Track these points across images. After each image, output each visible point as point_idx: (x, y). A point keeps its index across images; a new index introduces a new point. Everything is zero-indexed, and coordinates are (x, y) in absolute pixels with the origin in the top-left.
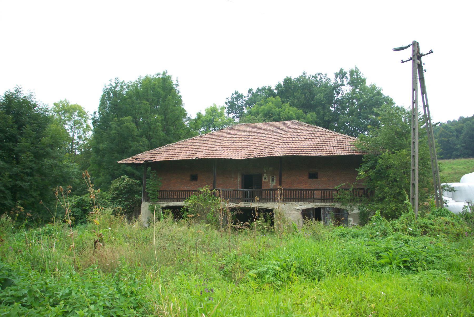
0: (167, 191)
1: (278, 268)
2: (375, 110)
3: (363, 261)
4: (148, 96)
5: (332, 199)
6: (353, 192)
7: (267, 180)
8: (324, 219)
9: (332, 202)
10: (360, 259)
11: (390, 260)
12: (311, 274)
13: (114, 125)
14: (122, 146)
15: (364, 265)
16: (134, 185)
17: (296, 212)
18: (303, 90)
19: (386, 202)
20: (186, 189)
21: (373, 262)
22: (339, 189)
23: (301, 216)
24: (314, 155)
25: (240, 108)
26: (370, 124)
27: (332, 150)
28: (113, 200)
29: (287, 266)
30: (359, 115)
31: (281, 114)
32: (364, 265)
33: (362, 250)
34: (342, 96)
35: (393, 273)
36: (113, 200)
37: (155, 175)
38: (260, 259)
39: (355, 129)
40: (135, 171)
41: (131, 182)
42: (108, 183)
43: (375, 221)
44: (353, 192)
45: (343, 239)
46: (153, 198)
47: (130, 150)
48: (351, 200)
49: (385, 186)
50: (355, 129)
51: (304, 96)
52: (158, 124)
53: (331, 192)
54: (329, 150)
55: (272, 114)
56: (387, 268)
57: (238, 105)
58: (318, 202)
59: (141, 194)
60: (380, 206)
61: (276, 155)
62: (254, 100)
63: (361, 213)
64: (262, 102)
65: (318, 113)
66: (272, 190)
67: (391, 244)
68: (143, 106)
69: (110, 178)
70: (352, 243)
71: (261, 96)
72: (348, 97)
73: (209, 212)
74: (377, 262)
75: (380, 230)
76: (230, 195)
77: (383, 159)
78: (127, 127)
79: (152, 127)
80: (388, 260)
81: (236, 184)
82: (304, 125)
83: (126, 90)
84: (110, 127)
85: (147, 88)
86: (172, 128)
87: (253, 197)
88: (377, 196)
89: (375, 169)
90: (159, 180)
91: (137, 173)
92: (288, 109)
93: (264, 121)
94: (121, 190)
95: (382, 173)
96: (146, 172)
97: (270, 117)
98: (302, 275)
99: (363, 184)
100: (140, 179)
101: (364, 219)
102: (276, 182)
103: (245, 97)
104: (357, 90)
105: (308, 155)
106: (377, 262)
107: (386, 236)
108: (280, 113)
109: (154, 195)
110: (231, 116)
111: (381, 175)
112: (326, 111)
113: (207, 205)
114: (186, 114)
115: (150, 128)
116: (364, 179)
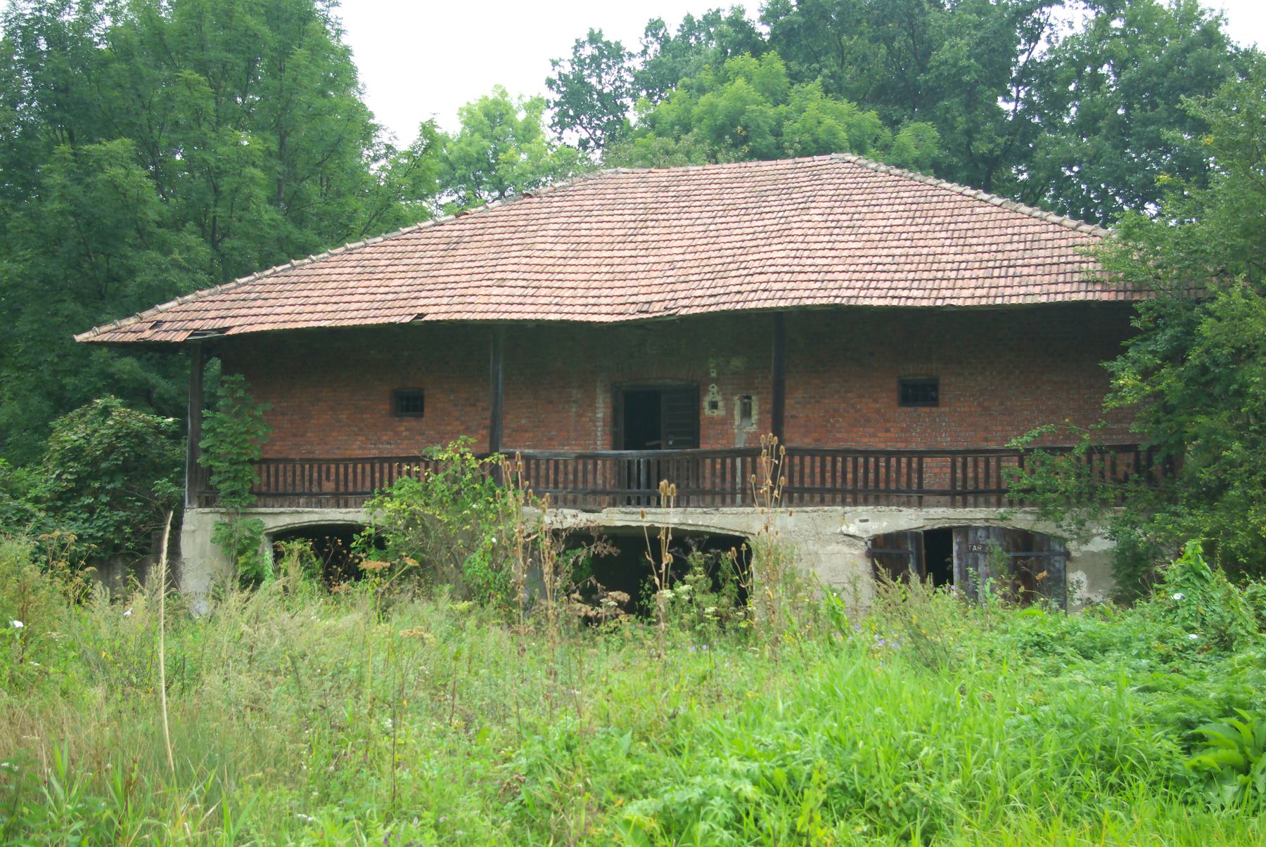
0: (292, 461)
1: (748, 790)
2: (1191, 104)
3: (1124, 760)
4: (202, 48)
5: (1000, 492)
6: (1090, 461)
7: (720, 412)
8: (965, 576)
9: (999, 505)
10: (1113, 748)
11: (1243, 752)
12: (896, 817)
13: (57, 179)
14: (95, 267)
15: (1128, 775)
16: (150, 439)
17: (845, 549)
18: (879, 22)
19: (1233, 505)
20: (374, 453)
21: (1165, 764)
22: (1029, 451)
23: (864, 566)
24: (925, 303)
25: (611, 103)
26: (1169, 170)
27: (1002, 282)
28: (60, 503)
29: (791, 779)
30: (1121, 130)
31: (787, 127)
32: (1128, 775)
33: (1121, 708)
34: (1051, 51)
35: (1255, 813)
36: (60, 503)
37: (240, 393)
38: (677, 752)
39: (1103, 195)
40: (154, 378)
41: (136, 425)
42: (36, 430)
43: (1179, 587)
44: (1090, 461)
45: (1039, 660)
46: (233, 494)
47: (131, 288)
48: (1080, 495)
49: (1226, 436)
50: (1103, 195)
51: (883, 50)
52: (250, 171)
53: (993, 463)
54: (987, 283)
55: (745, 128)
56: (1229, 790)
57: (600, 93)
58: (938, 505)
59: (182, 474)
60: (1204, 520)
61: (761, 305)
62: (673, 70)
63: (1122, 552)
64: (706, 77)
65: (945, 125)
66: (743, 453)
67: (1249, 686)
68: (182, 92)
69: (46, 406)
70: (1079, 678)
71: (699, 53)
72: (1077, 53)
73: (471, 550)
74: (1185, 764)
75: (1203, 623)
76: (561, 478)
77: (1219, 319)
78: (113, 185)
79: (226, 184)
80: (1233, 755)
81: (592, 428)
82: (877, 174)
83: (108, 21)
84: (39, 186)
85: (200, 16)
86: (312, 189)
87: (652, 484)
88: (1194, 481)
89: (1184, 361)
90: (259, 413)
91: (163, 386)
92: (817, 107)
93: (713, 158)
94: (95, 462)
95: (1216, 379)
96: (201, 381)
97: (738, 142)
98: (855, 818)
99: (1134, 428)
100: (178, 412)
101: (1134, 577)
102: (760, 422)
103: (631, 55)
104: (1117, 24)
105: (895, 302)
106: (1185, 764)
107: (1226, 649)
108: (780, 125)
109: (235, 479)
110: (572, 137)
111: (1210, 387)
112: (980, 113)
113: (465, 520)
114: (376, 128)
115: (216, 189)
116: (1134, 408)
